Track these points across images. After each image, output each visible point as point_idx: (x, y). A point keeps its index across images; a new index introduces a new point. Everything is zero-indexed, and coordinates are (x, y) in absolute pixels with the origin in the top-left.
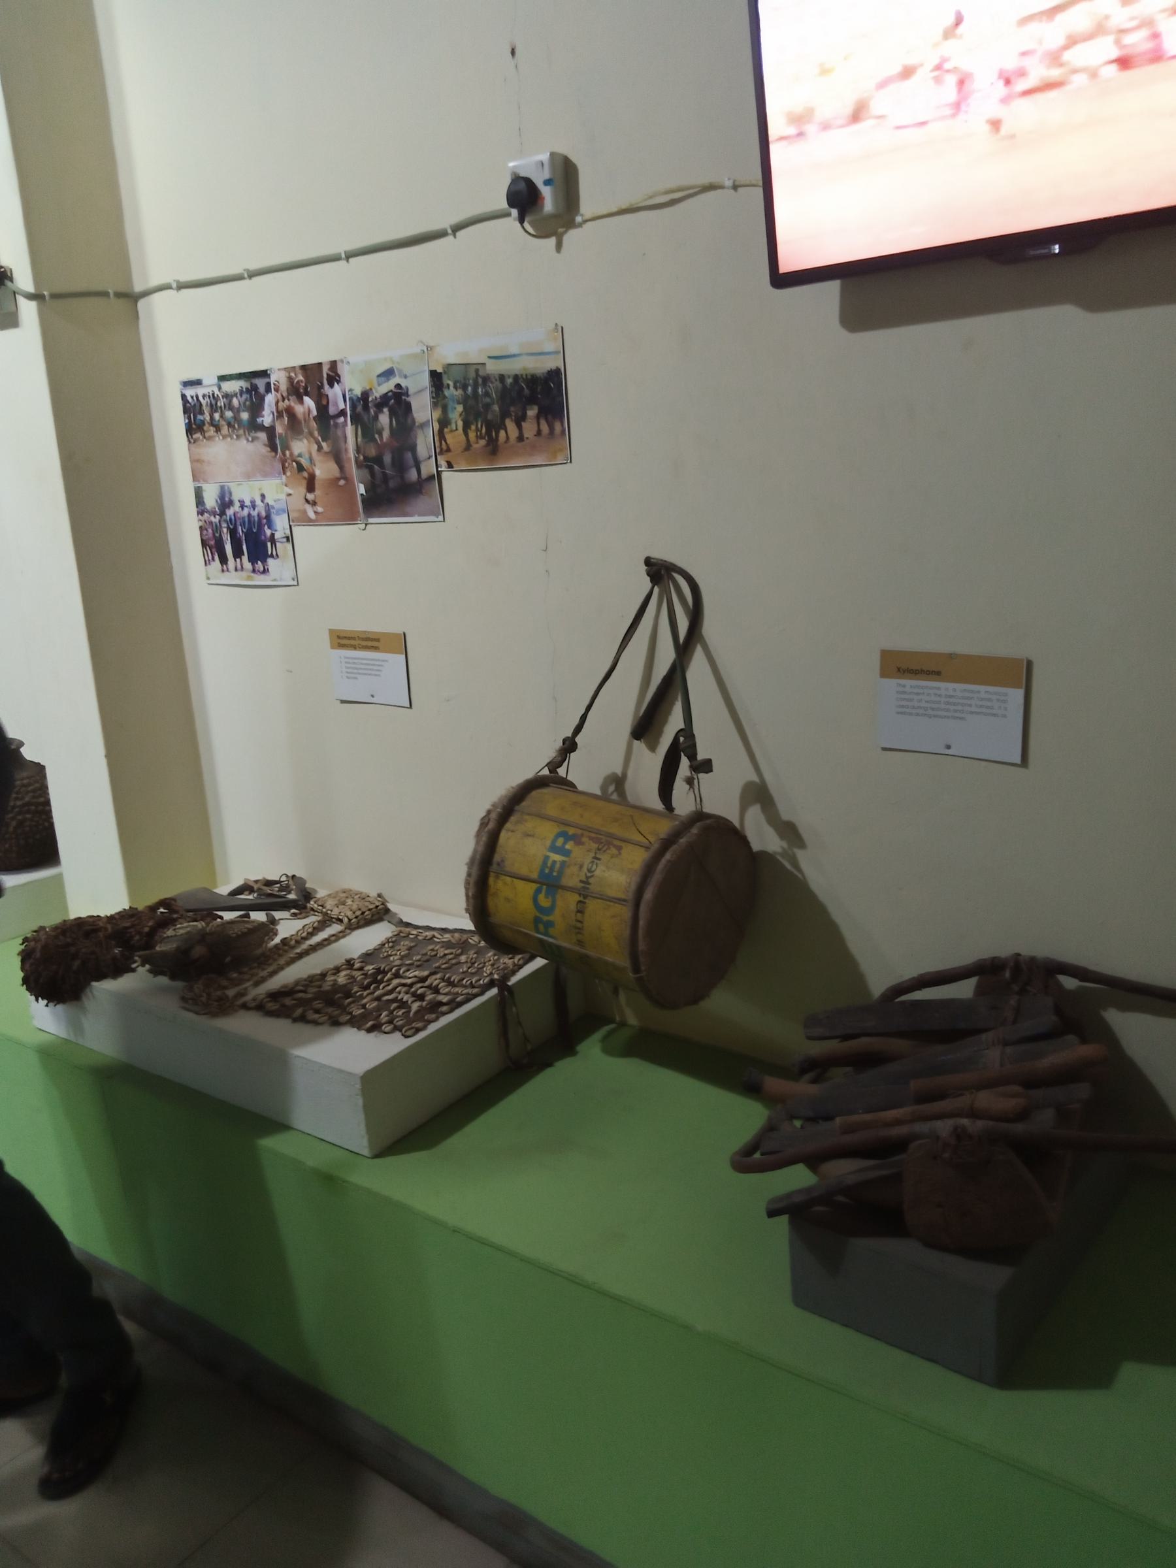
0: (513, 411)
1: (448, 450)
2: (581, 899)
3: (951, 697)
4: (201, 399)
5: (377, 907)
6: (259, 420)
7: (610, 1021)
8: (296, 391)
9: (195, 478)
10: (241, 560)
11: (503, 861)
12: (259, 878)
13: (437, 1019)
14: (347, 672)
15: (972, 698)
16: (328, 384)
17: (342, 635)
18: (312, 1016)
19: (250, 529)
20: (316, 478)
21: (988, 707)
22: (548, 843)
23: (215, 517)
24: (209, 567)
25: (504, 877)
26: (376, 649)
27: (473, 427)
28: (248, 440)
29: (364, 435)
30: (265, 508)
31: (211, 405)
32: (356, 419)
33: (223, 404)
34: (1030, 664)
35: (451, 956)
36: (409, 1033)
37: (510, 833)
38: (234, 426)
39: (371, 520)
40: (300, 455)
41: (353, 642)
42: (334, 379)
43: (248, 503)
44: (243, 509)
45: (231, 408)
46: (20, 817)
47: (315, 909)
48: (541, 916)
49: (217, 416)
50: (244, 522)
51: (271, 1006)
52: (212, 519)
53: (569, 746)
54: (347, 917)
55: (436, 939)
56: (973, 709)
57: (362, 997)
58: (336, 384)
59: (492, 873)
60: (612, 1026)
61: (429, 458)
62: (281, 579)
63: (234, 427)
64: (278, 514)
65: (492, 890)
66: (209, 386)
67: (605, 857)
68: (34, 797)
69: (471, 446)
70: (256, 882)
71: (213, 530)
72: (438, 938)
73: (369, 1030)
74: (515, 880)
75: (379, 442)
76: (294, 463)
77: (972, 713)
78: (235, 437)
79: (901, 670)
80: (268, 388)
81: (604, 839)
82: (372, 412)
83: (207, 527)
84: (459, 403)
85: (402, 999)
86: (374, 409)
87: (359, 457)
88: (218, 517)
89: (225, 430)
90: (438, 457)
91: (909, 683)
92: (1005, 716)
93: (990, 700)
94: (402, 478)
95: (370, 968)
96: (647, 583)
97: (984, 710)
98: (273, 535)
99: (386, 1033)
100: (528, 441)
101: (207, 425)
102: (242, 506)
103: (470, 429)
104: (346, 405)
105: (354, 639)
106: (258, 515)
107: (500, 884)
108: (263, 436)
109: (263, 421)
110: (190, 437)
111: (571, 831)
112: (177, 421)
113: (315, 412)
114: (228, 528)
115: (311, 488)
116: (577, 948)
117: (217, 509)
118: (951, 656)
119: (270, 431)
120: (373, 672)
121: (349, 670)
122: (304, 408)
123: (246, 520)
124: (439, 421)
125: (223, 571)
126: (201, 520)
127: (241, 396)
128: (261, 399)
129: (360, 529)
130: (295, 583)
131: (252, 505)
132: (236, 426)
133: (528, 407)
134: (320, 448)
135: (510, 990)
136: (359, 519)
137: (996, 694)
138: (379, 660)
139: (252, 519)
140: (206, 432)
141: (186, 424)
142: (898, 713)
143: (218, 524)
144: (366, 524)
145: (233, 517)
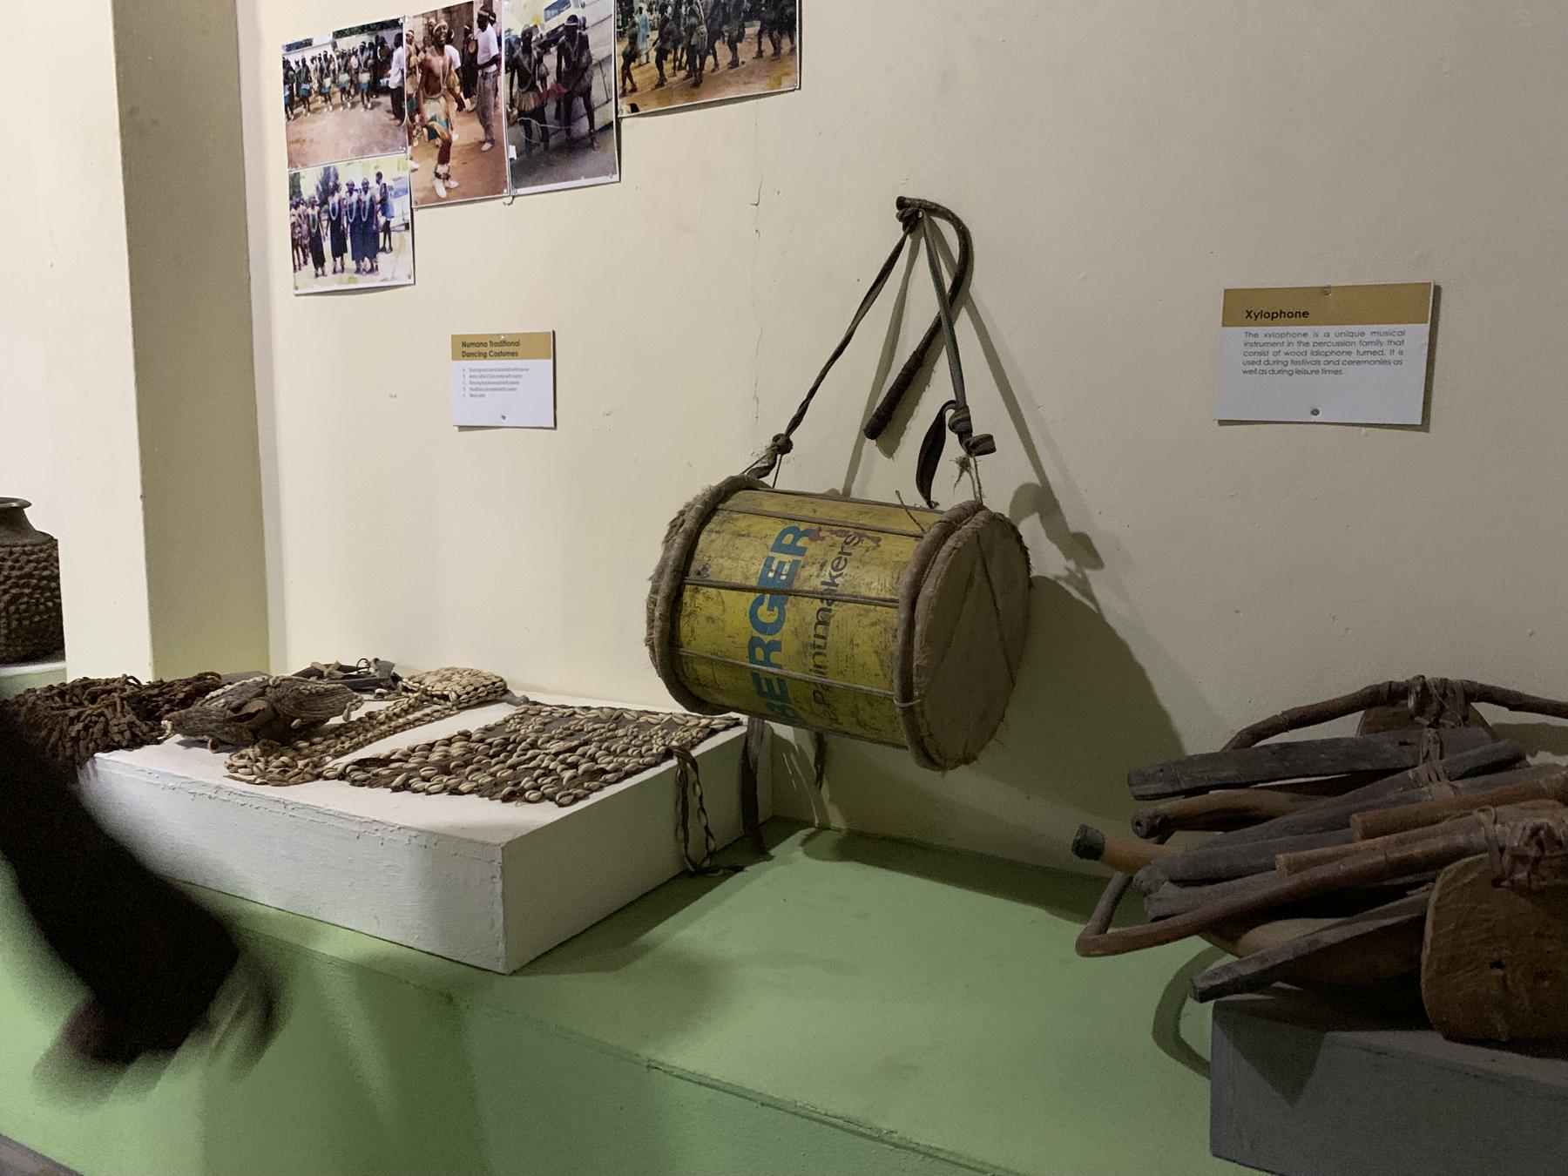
0: (726, 31)
1: (634, 90)
2: (825, 605)
3: (1320, 344)
4: (308, 63)
5: (494, 683)
6: (383, 81)
7: (809, 824)
8: (436, 40)
9: (291, 163)
10: (342, 259)
11: (705, 568)
12: (332, 662)
13: (601, 788)
14: (471, 389)
15: (1351, 344)
16: (479, 27)
17: (469, 341)
18: (416, 783)
19: (359, 217)
20: (453, 144)
21: (1374, 353)
22: (771, 543)
23: (313, 208)
24: (298, 273)
25: (706, 589)
26: (514, 355)
27: (670, 57)
28: (366, 107)
29: (521, 85)
30: (381, 190)
31: (322, 70)
32: (513, 65)
33: (337, 66)
34: (1437, 289)
35: (603, 731)
36: (566, 800)
37: (714, 536)
38: (349, 91)
39: (520, 191)
40: (433, 119)
41: (483, 349)
42: (487, 19)
43: (358, 186)
44: (351, 194)
45: (347, 69)
46: (14, 591)
47: (410, 688)
48: (761, 636)
49: (328, 82)
50: (351, 211)
51: (360, 776)
52: (310, 211)
53: (782, 445)
54: (456, 692)
55: (577, 716)
56: (1354, 357)
57: (489, 765)
58: (489, 25)
59: (688, 587)
60: (813, 829)
61: (607, 102)
62: (393, 278)
63: (349, 93)
64: (396, 195)
65: (687, 609)
66: (323, 43)
67: (857, 552)
68: (36, 569)
69: (666, 80)
70: (327, 666)
71: (308, 225)
72: (580, 714)
73: (506, 799)
74: (722, 591)
75: (541, 90)
76: (425, 130)
77: (1350, 363)
78: (349, 105)
79: (1252, 314)
80: (398, 43)
81: (852, 531)
82: (535, 53)
83: (301, 222)
84: (653, 29)
85: (548, 766)
86: (539, 50)
87: (512, 112)
88: (317, 208)
89: (337, 98)
90: (619, 100)
91: (1262, 331)
92: (1400, 362)
93: (1378, 343)
94: (568, 132)
95: (497, 740)
96: (898, 229)
97: (1369, 357)
98: (388, 223)
99: (530, 802)
100: (744, 66)
101: (314, 95)
102: (351, 191)
103: (666, 60)
104: (500, 50)
105: (485, 345)
106: (371, 200)
107: (700, 597)
108: (386, 100)
109: (388, 82)
110: (290, 113)
111: (803, 527)
112: (275, 92)
113: (459, 64)
114: (330, 219)
115: (444, 158)
116: (814, 677)
117: (317, 199)
118: (1325, 291)
119: (397, 94)
120: (506, 386)
121: (474, 386)
122: (444, 60)
123: (355, 207)
124: (625, 55)
125: (317, 276)
126: (294, 215)
127: (362, 54)
128: (389, 55)
129: (504, 203)
130: (412, 281)
131: (364, 189)
132: (352, 92)
133: (746, 24)
134: (461, 106)
135: (693, 762)
136: (505, 191)
137: (1386, 334)
138: (515, 369)
139: (363, 205)
140: (312, 103)
141: (285, 97)
142: (1245, 372)
143: (316, 217)
144: (514, 197)
145: (337, 207)
